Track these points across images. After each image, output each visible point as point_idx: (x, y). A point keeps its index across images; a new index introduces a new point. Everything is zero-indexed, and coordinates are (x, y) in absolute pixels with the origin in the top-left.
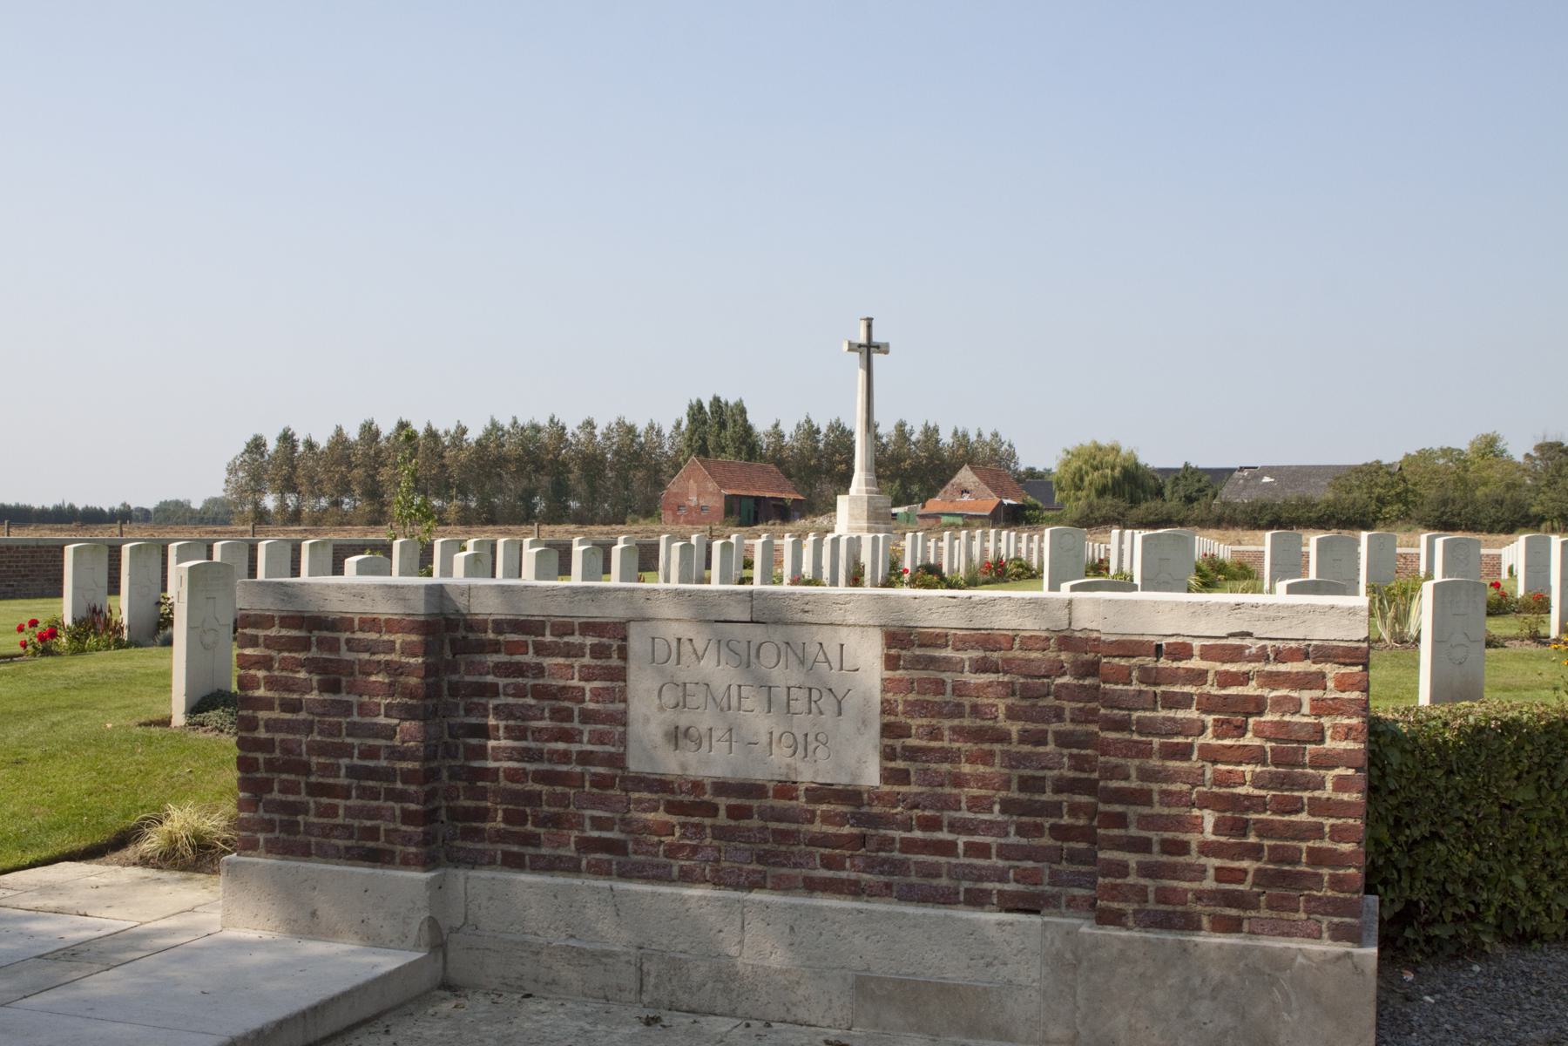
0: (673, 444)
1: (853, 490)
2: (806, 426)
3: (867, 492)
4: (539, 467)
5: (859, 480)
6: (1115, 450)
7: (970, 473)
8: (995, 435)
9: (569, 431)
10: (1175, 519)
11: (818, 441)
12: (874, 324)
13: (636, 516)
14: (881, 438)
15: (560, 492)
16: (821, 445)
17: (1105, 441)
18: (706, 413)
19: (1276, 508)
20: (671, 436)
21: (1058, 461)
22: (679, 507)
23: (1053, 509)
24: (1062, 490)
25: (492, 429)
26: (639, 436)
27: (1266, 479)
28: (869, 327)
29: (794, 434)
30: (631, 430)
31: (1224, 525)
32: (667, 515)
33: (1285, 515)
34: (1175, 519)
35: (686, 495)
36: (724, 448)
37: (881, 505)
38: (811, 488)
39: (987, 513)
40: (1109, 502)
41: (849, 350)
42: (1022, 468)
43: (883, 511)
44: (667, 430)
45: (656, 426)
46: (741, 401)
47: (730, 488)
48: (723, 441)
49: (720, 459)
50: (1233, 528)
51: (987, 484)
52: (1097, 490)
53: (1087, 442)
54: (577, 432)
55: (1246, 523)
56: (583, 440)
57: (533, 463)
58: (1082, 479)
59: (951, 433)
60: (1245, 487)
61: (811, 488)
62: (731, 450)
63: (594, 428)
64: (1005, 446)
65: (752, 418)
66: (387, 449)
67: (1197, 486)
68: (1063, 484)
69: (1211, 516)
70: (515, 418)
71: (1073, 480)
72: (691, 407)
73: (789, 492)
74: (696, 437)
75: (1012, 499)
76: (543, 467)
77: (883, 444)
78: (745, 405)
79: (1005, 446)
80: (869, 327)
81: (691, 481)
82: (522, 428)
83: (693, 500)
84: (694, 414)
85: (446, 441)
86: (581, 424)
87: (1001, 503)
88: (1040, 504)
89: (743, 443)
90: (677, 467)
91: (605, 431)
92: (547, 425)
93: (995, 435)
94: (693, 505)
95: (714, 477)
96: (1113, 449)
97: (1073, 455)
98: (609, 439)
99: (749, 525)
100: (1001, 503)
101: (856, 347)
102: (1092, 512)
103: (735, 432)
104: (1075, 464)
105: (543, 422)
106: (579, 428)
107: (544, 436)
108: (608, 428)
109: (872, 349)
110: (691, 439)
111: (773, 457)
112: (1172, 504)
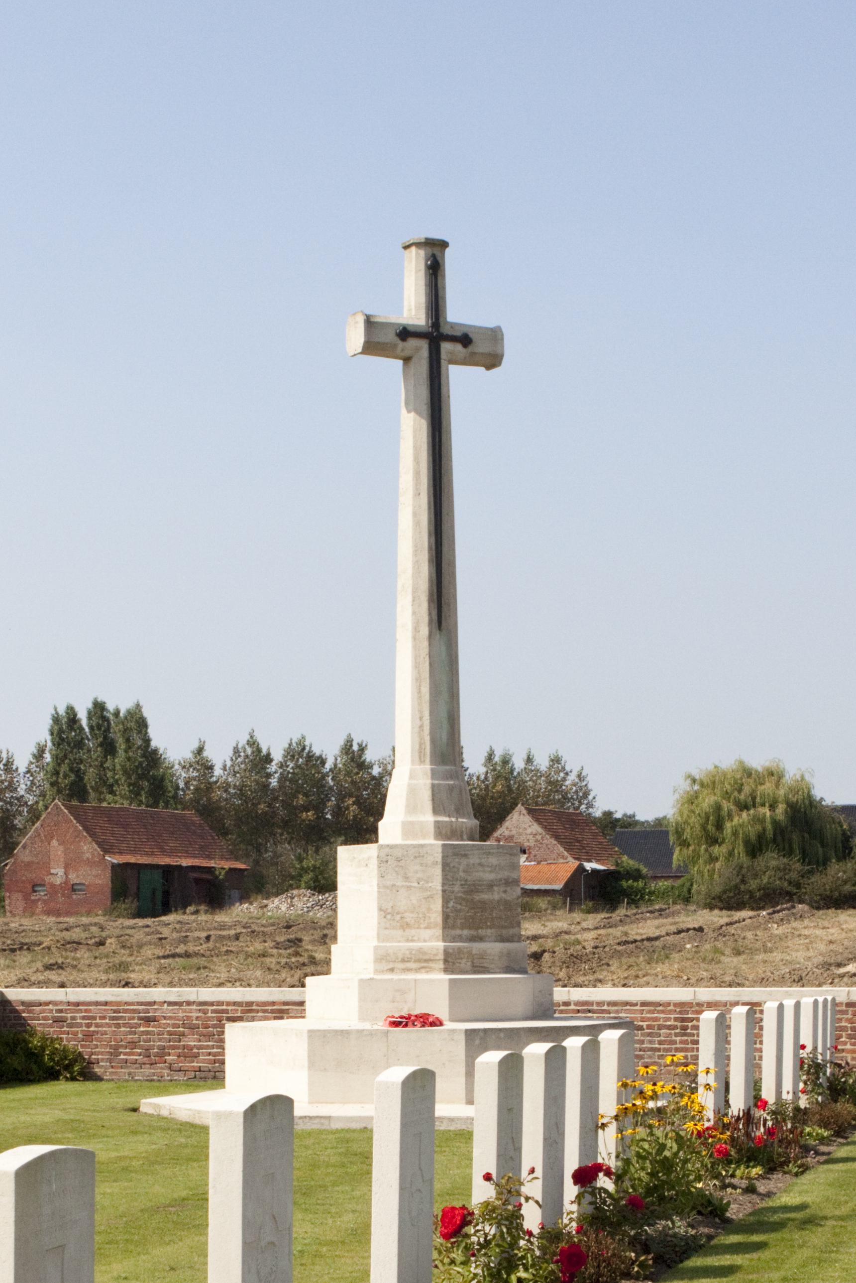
0: (32, 782)
2: (249, 751)
3: (441, 831)
5: (412, 791)
6: (774, 774)
7: (527, 819)
8: (556, 760)
11: (269, 776)
14: (370, 766)
16: (274, 782)
17: (758, 763)
18: (81, 728)
20: (28, 772)
21: (677, 796)
22: (34, 887)
23: (669, 877)
24: (685, 844)
29: (229, 763)
35: (46, 866)
37: (489, 876)
39: (558, 886)
40: (773, 863)
41: (371, 347)
42: (597, 813)
44: (22, 762)
46: (138, 706)
47: (121, 853)
49: (105, 804)
51: (557, 837)
52: (747, 842)
58: (719, 826)
59: (482, 759)
61: (259, 851)
62: (123, 789)
64: (572, 778)
65: (158, 738)
68: (687, 834)
71: (704, 828)
72: (56, 719)
73: (222, 858)
74: (64, 768)
75: (598, 861)
77: (374, 778)
78: (146, 713)
79: (572, 778)
81: (54, 842)
83: (58, 875)
84: (61, 731)
87: (581, 869)
88: (644, 870)
89: (142, 777)
90: (35, 815)
93: (556, 760)
94: (58, 881)
95: (93, 835)
96: (772, 774)
97: (702, 785)
99: (154, 915)
100: (581, 869)
101: (390, 337)
102: (743, 881)
104: (707, 801)
109: (446, 347)
110: (57, 773)
111: (196, 801)
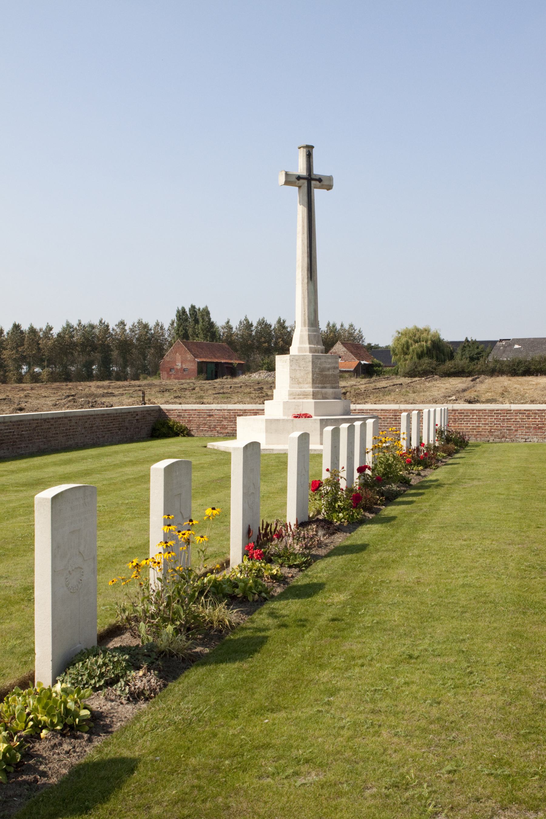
0: (170, 333)
1: (294, 349)
2: (245, 322)
3: (311, 350)
4: (94, 348)
5: (301, 336)
6: (427, 331)
7: (341, 346)
8: (351, 326)
9: (111, 328)
10: (467, 371)
11: (252, 331)
12: (315, 152)
13: (146, 375)
15: (106, 362)
16: (254, 333)
17: (421, 326)
19: (527, 363)
21: (393, 338)
22: (171, 370)
23: (390, 366)
24: (396, 355)
25: (67, 327)
26: (151, 330)
27: (516, 346)
28: (309, 156)
29: (238, 327)
30: (146, 326)
31: (496, 374)
32: (164, 374)
33: (533, 367)
34: (467, 371)
35: (175, 362)
36: (197, 335)
38: (248, 357)
39: (352, 369)
40: (427, 361)
41: (287, 183)
42: (366, 344)
43: (330, 372)
44: (166, 326)
45: (160, 324)
46: (207, 307)
47: (201, 358)
48: (197, 330)
50: (502, 376)
51: (352, 352)
52: (417, 354)
53: (410, 326)
54: (115, 328)
55: (510, 372)
56: (118, 332)
57: (90, 346)
58: (408, 348)
59: (326, 325)
60: (504, 351)
61: (248, 357)
62: (201, 336)
63: (125, 325)
64: (357, 332)
65: (214, 318)
66: (7, 339)
67: (476, 351)
68: (397, 351)
69: (488, 369)
70: (79, 321)
71: (402, 349)
73: (236, 359)
74: (181, 328)
75: (366, 361)
76: (96, 349)
77: (288, 332)
79: (357, 332)
80: (309, 156)
81: (178, 354)
82: (84, 326)
83: (179, 365)
84: (180, 316)
85: (41, 334)
86: (117, 323)
87: (360, 363)
88: (382, 364)
89: (208, 331)
90: (171, 345)
91: (131, 327)
92: (98, 324)
93: (351, 326)
97: (402, 334)
98: (133, 331)
100: (360, 363)
101: (294, 179)
103: (203, 325)
104: (404, 340)
105: (96, 322)
106: (116, 325)
107: (97, 331)
108: (133, 325)
109: (313, 182)
110: (178, 330)
112: (460, 361)
